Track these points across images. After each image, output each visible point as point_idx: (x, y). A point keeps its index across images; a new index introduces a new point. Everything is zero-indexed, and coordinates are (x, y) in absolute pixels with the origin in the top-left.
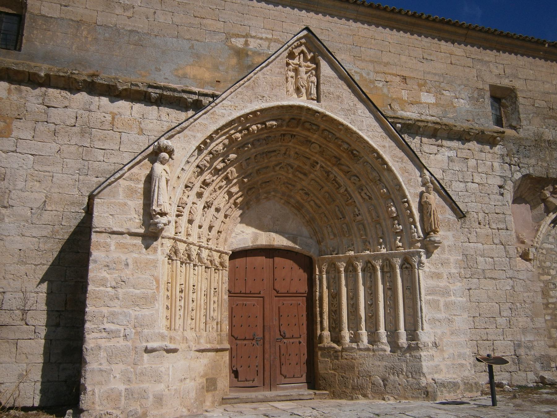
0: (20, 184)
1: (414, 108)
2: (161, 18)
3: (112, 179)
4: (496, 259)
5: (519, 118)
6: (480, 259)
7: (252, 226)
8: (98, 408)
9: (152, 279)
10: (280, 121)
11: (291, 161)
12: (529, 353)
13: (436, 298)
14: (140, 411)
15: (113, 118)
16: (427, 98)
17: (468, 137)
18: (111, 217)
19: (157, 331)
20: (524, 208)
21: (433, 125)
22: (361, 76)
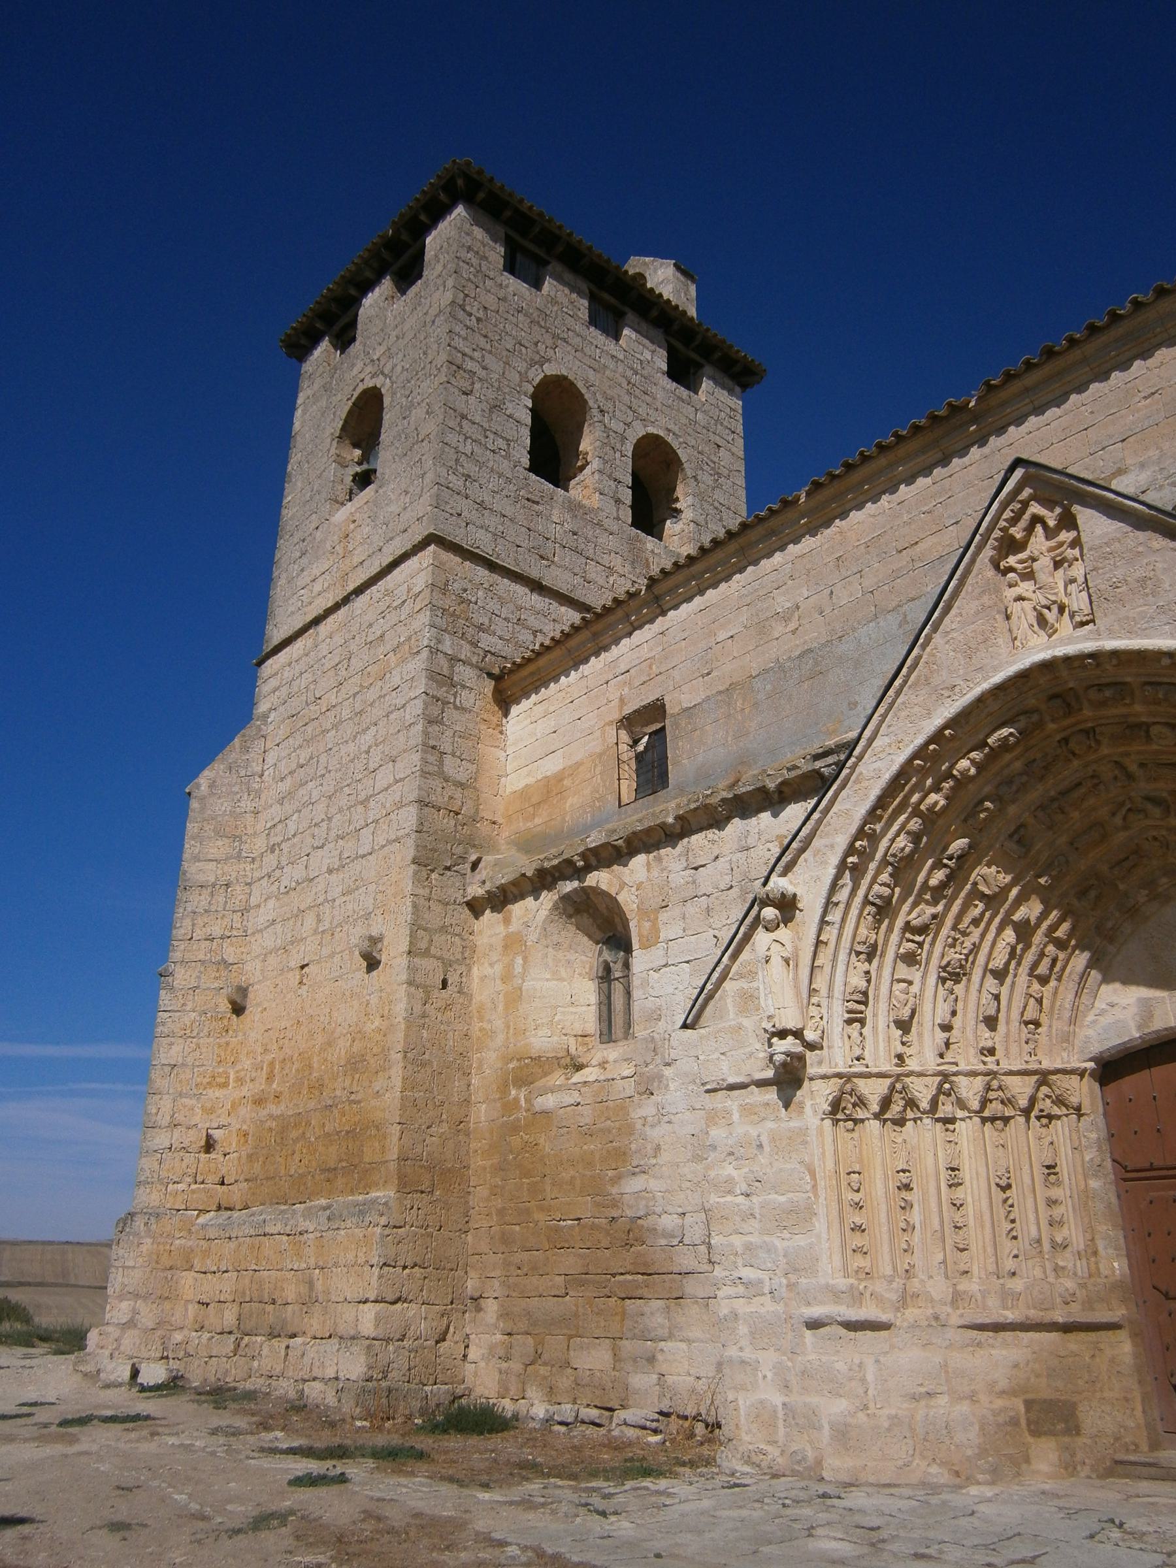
2: (842, 597)
7: (1137, 983)
9: (803, 1169)
10: (1021, 718)
18: (723, 1057)
19: (822, 1281)
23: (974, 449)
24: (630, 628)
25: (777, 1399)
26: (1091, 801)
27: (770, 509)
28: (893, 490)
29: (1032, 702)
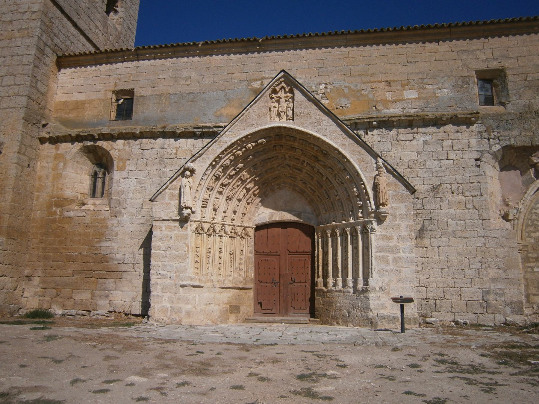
0: (130, 196)
1: (398, 105)
2: (207, 80)
3: (161, 190)
4: (467, 221)
5: (508, 95)
6: (451, 222)
7: (271, 208)
8: (157, 315)
11: (288, 162)
12: (498, 299)
13: (385, 254)
14: (178, 319)
15: (177, 151)
16: (410, 94)
17: (442, 122)
20: (514, 175)
21: (406, 118)
22: (350, 88)
23: (256, 53)
24: (123, 60)
25: (169, 305)
26: (274, 162)
27: (189, 44)
28: (229, 54)
29: (272, 135)
